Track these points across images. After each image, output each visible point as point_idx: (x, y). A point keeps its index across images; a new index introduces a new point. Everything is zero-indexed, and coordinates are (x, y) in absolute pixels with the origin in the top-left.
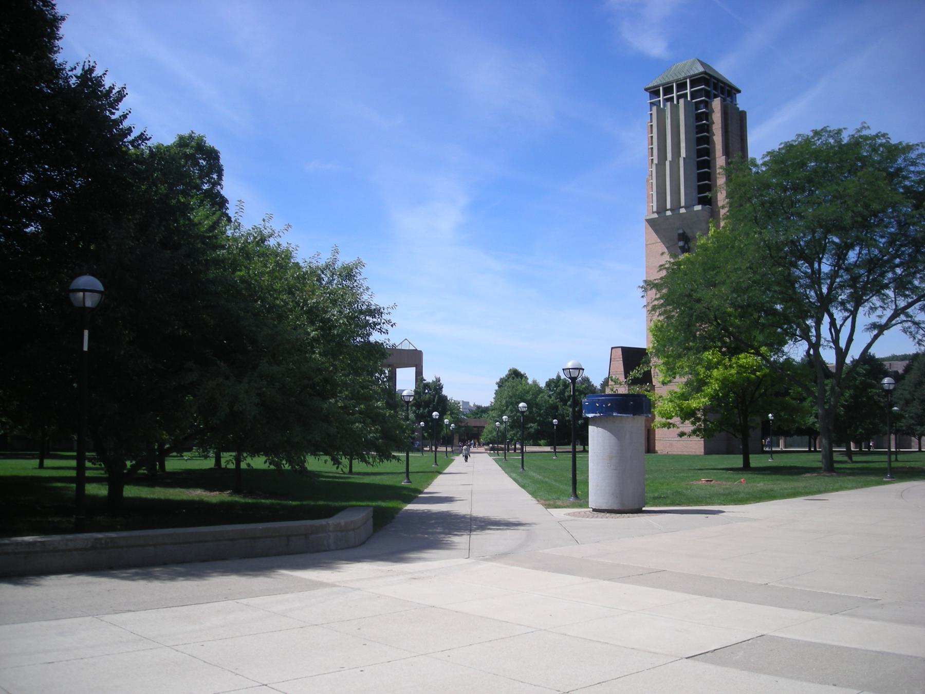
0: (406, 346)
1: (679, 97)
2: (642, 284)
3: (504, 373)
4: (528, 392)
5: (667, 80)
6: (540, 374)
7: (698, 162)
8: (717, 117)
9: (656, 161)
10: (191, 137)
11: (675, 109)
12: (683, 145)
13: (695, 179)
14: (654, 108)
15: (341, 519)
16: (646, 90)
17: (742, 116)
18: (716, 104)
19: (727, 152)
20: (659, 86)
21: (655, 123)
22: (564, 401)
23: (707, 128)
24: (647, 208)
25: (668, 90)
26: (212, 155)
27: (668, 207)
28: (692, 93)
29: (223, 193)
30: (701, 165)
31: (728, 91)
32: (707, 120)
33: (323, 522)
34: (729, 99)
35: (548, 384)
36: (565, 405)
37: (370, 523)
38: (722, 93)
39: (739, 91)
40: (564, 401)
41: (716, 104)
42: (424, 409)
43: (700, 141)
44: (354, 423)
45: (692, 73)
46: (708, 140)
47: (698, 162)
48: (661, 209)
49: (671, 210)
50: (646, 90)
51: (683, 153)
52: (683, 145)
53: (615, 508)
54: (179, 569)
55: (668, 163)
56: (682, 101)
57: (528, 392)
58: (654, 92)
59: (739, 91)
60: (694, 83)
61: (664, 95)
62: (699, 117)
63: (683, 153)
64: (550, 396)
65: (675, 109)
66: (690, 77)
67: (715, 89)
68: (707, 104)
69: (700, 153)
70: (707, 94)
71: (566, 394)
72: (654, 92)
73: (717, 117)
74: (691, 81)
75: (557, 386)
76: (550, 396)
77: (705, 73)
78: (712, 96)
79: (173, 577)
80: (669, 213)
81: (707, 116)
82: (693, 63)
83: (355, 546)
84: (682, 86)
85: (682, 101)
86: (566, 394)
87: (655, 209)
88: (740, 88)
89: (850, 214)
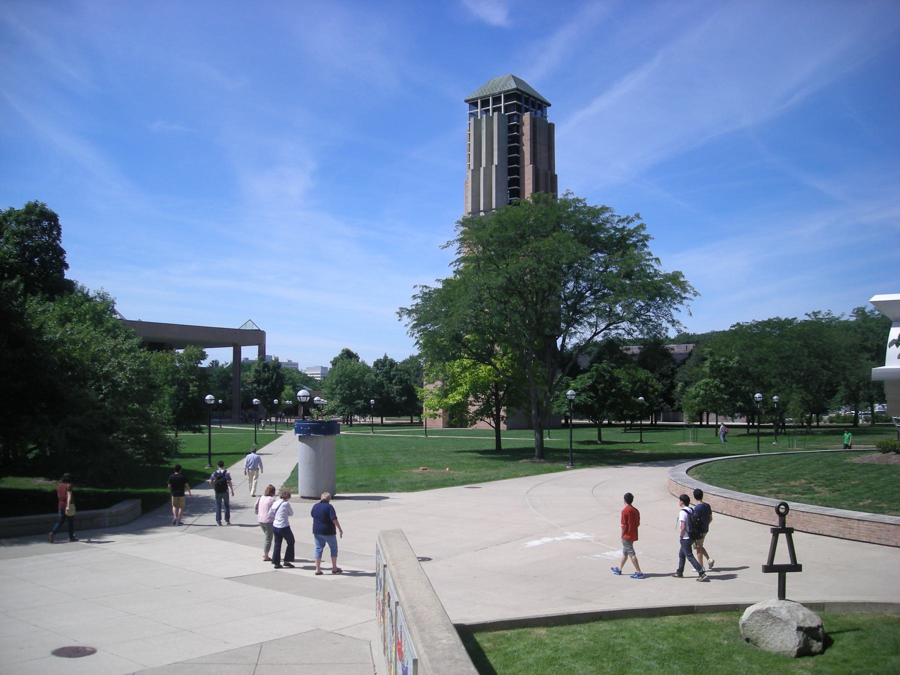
0: (249, 327)
1: (494, 110)
2: (398, 310)
3: (337, 353)
4: (356, 372)
5: (485, 94)
6: (369, 357)
7: (509, 169)
8: (526, 129)
9: (472, 167)
10: (36, 205)
11: (490, 121)
12: (496, 153)
13: (506, 183)
14: (472, 119)
15: (114, 509)
16: (466, 101)
17: (551, 128)
18: (526, 117)
19: (534, 161)
20: (477, 99)
21: (472, 132)
22: (390, 379)
23: (518, 139)
24: (464, 209)
25: (485, 103)
26: (53, 218)
27: (482, 209)
28: (505, 107)
29: (61, 245)
30: (511, 172)
31: (537, 105)
32: (518, 132)
33: (102, 511)
34: (539, 112)
35: (376, 364)
36: (391, 383)
37: (140, 508)
38: (533, 107)
39: (550, 105)
40: (390, 379)
41: (526, 117)
42: (264, 386)
43: (511, 150)
44: (128, 448)
45: (506, 89)
46: (518, 150)
47: (509, 169)
48: (475, 210)
49: (484, 211)
50: (466, 101)
51: (496, 162)
52: (496, 153)
53: (313, 496)
54: (16, 540)
55: (482, 169)
56: (496, 114)
57: (356, 372)
58: (473, 103)
59: (550, 105)
60: (508, 97)
61: (482, 107)
62: (511, 129)
63: (496, 162)
64: (377, 375)
65: (490, 121)
66: (504, 92)
67: (526, 103)
68: (519, 118)
69: (511, 161)
70: (519, 108)
71: (392, 373)
72: (473, 103)
73: (526, 129)
74: (505, 96)
75: (384, 366)
76: (377, 375)
77: (517, 89)
78: (523, 109)
79: (11, 544)
80: (482, 214)
81: (518, 128)
82: (508, 79)
83: (122, 524)
84: (497, 100)
85: (496, 114)
86: (392, 373)
87: (470, 210)
88: (549, 101)
89: (544, 266)
